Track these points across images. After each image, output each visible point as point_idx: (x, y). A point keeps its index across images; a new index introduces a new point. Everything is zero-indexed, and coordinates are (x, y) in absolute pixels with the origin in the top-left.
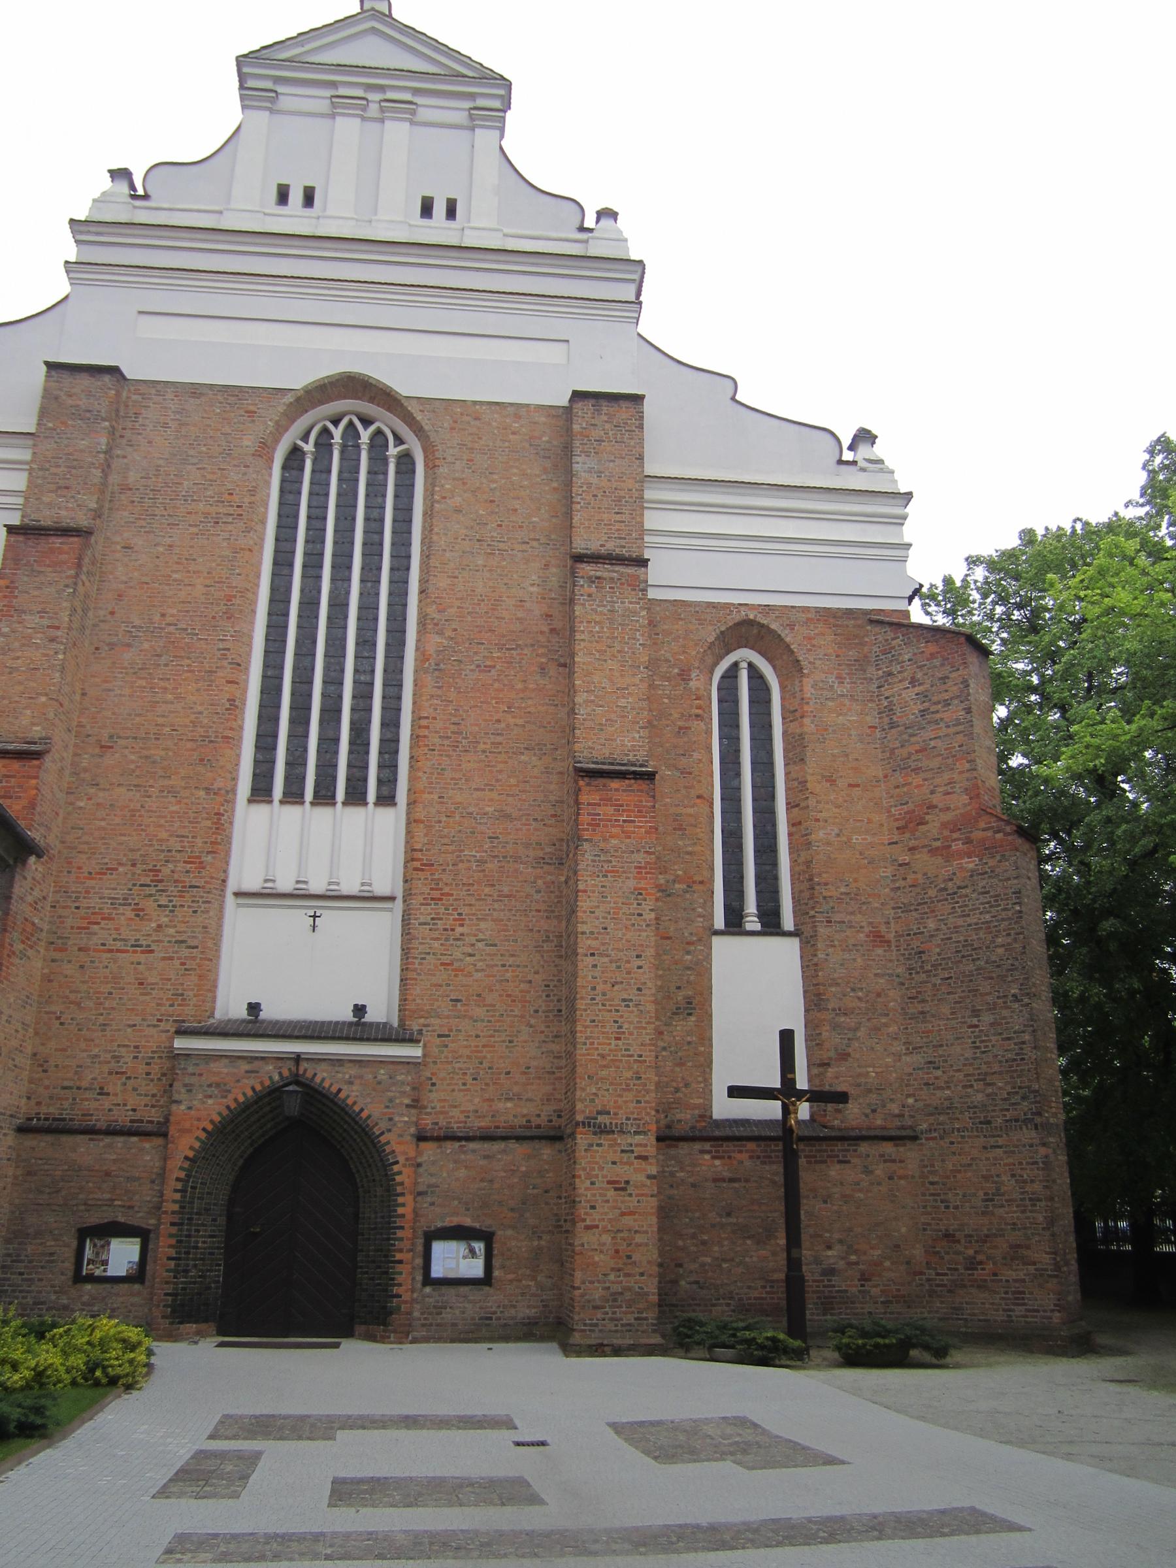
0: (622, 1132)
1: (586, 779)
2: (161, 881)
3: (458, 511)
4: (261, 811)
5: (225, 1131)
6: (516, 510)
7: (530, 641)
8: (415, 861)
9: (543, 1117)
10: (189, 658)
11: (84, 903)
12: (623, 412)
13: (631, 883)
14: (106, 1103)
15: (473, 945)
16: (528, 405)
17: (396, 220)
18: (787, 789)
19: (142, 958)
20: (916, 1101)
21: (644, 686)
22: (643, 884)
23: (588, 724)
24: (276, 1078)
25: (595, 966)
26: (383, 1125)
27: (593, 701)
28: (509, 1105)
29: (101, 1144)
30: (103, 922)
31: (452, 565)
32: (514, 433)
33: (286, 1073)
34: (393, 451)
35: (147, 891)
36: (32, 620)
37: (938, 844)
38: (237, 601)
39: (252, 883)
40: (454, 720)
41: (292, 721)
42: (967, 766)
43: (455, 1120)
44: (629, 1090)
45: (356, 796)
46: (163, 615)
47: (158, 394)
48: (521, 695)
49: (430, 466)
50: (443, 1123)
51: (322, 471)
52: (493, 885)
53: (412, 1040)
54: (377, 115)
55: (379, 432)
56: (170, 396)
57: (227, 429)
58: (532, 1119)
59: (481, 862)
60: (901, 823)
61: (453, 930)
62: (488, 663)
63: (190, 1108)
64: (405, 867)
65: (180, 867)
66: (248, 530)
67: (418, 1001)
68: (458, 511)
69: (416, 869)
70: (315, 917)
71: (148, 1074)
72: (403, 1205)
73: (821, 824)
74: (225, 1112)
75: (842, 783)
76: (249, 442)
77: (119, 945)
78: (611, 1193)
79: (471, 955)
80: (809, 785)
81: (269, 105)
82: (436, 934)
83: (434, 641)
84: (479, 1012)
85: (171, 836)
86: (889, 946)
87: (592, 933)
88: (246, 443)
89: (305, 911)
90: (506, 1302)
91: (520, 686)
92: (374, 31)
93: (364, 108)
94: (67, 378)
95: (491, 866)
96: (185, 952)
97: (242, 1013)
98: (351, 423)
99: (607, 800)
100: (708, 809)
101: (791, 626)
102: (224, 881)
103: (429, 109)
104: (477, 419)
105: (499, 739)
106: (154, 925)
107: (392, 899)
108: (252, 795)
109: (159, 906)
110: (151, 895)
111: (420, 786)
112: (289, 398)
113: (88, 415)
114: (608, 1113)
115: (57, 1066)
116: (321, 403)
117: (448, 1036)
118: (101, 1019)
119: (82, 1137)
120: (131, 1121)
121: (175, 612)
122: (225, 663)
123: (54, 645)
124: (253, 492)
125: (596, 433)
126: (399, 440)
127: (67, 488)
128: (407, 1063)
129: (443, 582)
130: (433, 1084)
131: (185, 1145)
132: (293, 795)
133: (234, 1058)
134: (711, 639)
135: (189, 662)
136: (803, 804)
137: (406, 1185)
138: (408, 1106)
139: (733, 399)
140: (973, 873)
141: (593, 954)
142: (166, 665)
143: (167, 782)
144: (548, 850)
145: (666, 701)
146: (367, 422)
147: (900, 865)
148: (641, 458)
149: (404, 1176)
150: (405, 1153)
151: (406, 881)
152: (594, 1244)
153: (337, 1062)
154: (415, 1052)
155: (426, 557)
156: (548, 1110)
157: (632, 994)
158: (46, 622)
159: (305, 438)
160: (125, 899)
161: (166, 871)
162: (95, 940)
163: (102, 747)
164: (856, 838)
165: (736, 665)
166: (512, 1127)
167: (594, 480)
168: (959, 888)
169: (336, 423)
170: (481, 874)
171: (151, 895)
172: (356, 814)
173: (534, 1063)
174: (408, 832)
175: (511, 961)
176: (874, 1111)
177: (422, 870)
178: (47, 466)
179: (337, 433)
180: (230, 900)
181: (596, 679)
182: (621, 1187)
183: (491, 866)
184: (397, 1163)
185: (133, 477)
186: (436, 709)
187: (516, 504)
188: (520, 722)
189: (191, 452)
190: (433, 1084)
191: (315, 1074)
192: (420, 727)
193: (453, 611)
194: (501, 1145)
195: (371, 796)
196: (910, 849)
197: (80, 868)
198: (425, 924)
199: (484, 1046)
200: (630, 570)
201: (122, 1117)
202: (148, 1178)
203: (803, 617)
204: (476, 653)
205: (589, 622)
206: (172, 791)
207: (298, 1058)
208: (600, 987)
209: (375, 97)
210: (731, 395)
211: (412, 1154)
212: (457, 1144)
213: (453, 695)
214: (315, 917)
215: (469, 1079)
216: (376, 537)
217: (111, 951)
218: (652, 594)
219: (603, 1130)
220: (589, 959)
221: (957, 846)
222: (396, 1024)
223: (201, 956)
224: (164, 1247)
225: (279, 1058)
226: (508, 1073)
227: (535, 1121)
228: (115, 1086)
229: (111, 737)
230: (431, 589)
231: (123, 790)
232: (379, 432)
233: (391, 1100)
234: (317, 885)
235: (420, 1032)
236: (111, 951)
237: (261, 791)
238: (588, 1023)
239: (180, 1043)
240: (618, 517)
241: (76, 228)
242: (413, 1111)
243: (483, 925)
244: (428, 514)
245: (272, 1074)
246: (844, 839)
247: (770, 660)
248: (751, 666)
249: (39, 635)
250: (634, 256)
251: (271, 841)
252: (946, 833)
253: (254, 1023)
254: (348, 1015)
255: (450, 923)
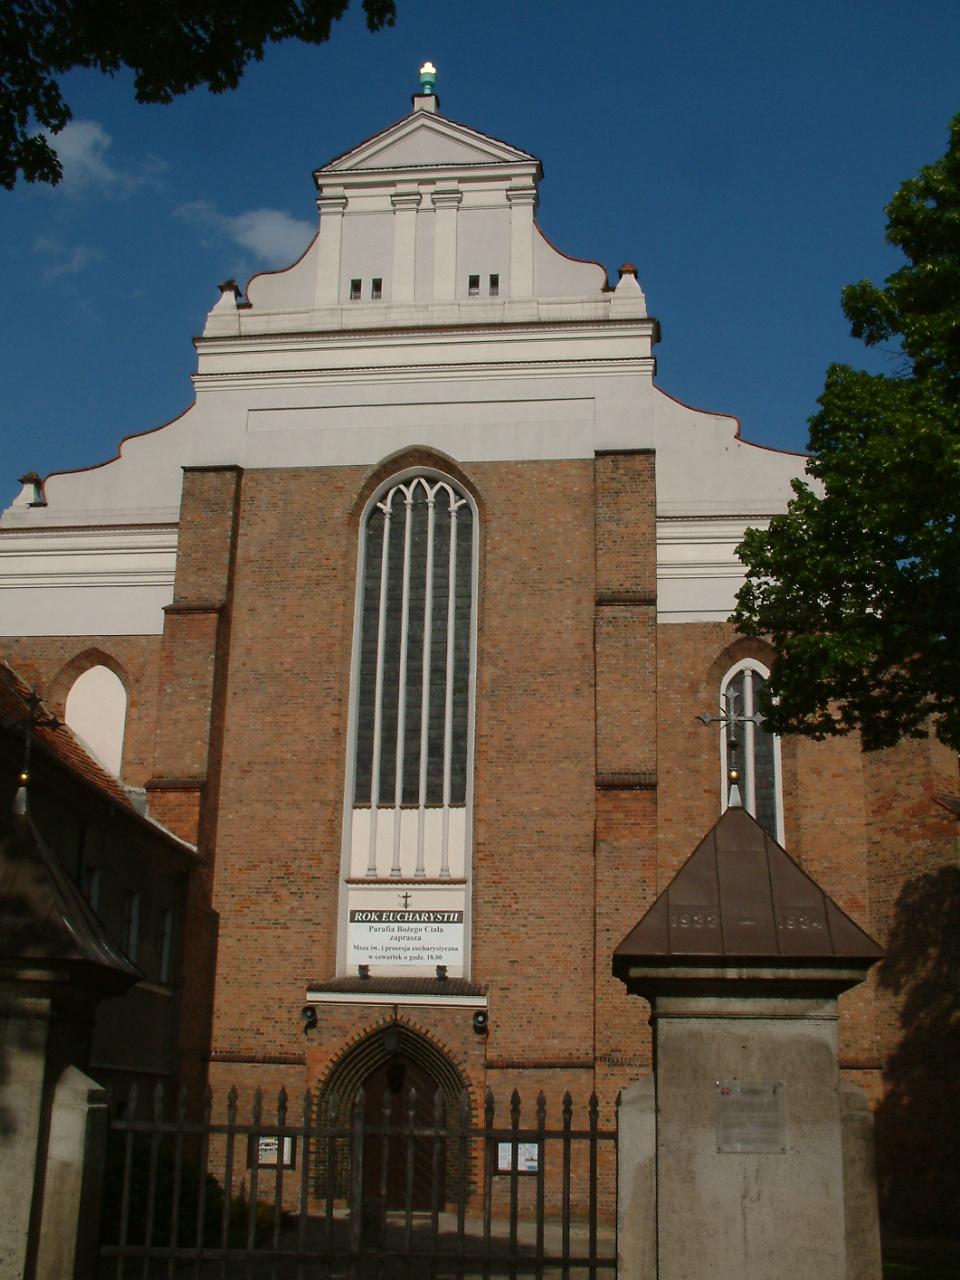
0: (630, 1065)
1: (603, 792)
2: (292, 874)
5: (345, 1064)
6: (553, 554)
7: (566, 667)
8: (481, 854)
9: (582, 1051)
10: (302, 697)
12: (638, 463)
13: (637, 874)
14: (262, 1040)
15: (526, 918)
16: (561, 461)
17: (447, 299)
18: (784, 779)
19: (280, 932)
20: (882, 1037)
22: (647, 874)
24: (381, 1022)
25: (609, 939)
26: (460, 1057)
27: (611, 723)
28: (556, 1042)
29: (260, 1070)
30: (252, 906)
31: (502, 606)
32: (549, 486)
33: (388, 1019)
35: (282, 882)
37: (902, 826)
39: (358, 870)
40: (507, 736)
42: (923, 761)
43: (515, 1053)
44: (636, 1033)
46: (282, 663)
48: (560, 713)
49: (483, 522)
50: (505, 1055)
52: (540, 870)
58: (574, 1052)
59: (530, 852)
60: (875, 808)
61: (510, 906)
62: (533, 687)
63: (320, 1044)
64: (473, 857)
65: (305, 863)
67: (485, 963)
69: (481, 859)
70: (406, 897)
71: (290, 1019)
72: (476, 1116)
73: (808, 810)
74: (345, 1048)
75: (827, 775)
76: (339, 514)
77: (264, 923)
79: (524, 926)
80: (799, 777)
81: (341, 209)
82: (498, 910)
83: (490, 672)
84: (531, 970)
85: (297, 839)
86: (865, 911)
87: (607, 913)
88: (337, 514)
89: (399, 893)
90: (555, 1189)
93: (419, 202)
95: (539, 855)
96: (311, 928)
98: (419, 483)
102: (338, 872)
103: (473, 194)
104: (518, 476)
105: (543, 751)
106: (288, 908)
108: (356, 801)
109: (291, 893)
110: (285, 885)
111: (482, 792)
112: (369, 473)
113: (216, 507)
114: (620, 1051)
115: (226, 1013)
117: (508, 989)
118: (255, 980)
119: (246, 1064)
120: (280, 1053)
121: (289, 660)
123: (203, 701)
127: (205, 569)
129: (495, 622)
130: (497, 1026)
132: (387, 799)
135: (302, 700)
136: (794, 793)
137: (479, 1101)
138: (478, 1043)
140: (926, 853)
141: (608, 930)
142: (286, 704)
144: (583, 840)
145: (679, 711)
146: (432, 481)
147: (874, 843)
150: (477, 1078)
151: (474, 868)
155: (482, 600)
158: (197, 683)
159: (383, 499)
160: (266, 889)
163: (243, 771)
164: (839, 821)
165: (741, 672)
166: (559, 1058)
167: (614, 527)
168: (915, 864)
169: (407, 484)
170: (532, 862)
171: (285, 885)
174: (475, 829)
176: (847, 1046)
177: (485, 859)
178: (189, 551)
179: (409, 493)
181: (614, 704)
183: (539, 855)
184: (471, 1085)
185: (253, 551)
186: (492, 728)
188: (560, 735)
189: (295, 526)
190: (497, 1026)
191: (409, 1020)
192: (481, 744)
193: (503, 645)
194: (550, 1072)
195: (200, 1241)
196: (881, 830)
197: (232, 865)
198: (488, 902)
199: (536, 996)
200: (643, 608)
204: (523, 680)
205: (606, 656)
211: (482, 1078)
212: (516, 1071)
214: (406, 897)
215: (525, 1023)
216: (443, 581)
217: (258, 928)
218: (661, 619)
220: (606, 935)
221: (915, 829)
222: (470, 980)
226: (554, 1017)
228: (267, 1027)
229: (249, 763)
230: (486, 629)
233: (466, 1039)
234: (408, 872)
235: (487, 988)
236: (258, 928)
238: (604, 983)
240: (634, 559)
242: (483, 1047)
243: (534, 902)
244: (483, 562)
245: (379, 1020)
246: (828, 822)
248: (754, 672)
249: (193, 694)
251: (378, 838)
252: (907, 818)
253: (365, 982)
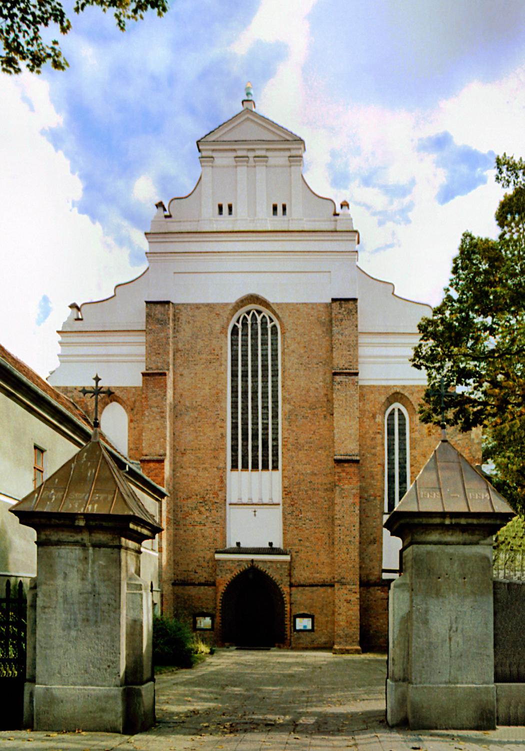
0: (349, 584)
3: (293, 352)
4: (235, 473)
8: (286, 492)
11: (183, 509)
12: (350, 305)
13: (352, 501)
19: (203, 528)
21: (358, 426)
23: (339, 441)
26: (280, 582)
34: (269, 326)
36: (155, 410)
38: (220, 395)
41: (243, 439)
45: (265, 467)
47: (185, 308)
49: (283, 333)
51: (245, 335)
53: (286, 554)
54: (254, 164)
55: (264, 317)
56: (189, 309)
57: (210, 323)
59: (306, 491)
65: (211, 496)
66: (221, 365)
68: (293, 352)
76: (218, 328)
77: (195, 523)
78: (345, 604)
84: (308, 544)
91: (317, 424)
92: (248, 119)
93: (248, 162)
94: (153, 306)
96: (215, 526)
97: (235, 545)
98: (254, 313)
99: (343, 471)
100: (382, 468)
101: (412, 394)
107: (279, 504)
112: (230, 307)
116: (242, 307)
122: (218, 420)
124: (221, 348)
125: (340, 316)
126: (272, 321)
128: (285, 562)
131: (222, 588)
133: (233, 561)
134: (383, 401)
139: (393, 293)
143: (204, 466)
148: (357, 326)
149: (287, 598)
152: (341, 620)
153: (264, 562)
154: (287, 558)
156: (330, 577)
157: (352, 539)
158: (159, 410)
159: (238, 322)
161: (207, 498)
162: (188, 522)
165: (394, 409)
172: (265, 473)
173: (325, 561)
175: (317, 526)
179: (249, 318)
180: (228, 506)
182: (348, 602)
187: (314, 348)
200: (353, 377)
201: (202, 580)
202: (212, 597)
203: (417, 389)
206: (206, 469)
207: (252, 561)
208: (342, 537)
209: (251, 154)
210: (391, 292)
213: (295, 429)
219: (343, 584)
220: (339, 528)
223: (221, 524)
224: (218, 620)
225: (247, 561)
227: (326, 580)
231: (190, 469)
232: (264, 317)
237: (234, 466)
239: (217, 556)
240: (349, 353)
241: (148, 236)
245: (246, 566)
247: (406, 408)
248: (399, 410)
250: (355, 229)
253: (239, 549)
254: (267, 546)
255: (297, 513)
